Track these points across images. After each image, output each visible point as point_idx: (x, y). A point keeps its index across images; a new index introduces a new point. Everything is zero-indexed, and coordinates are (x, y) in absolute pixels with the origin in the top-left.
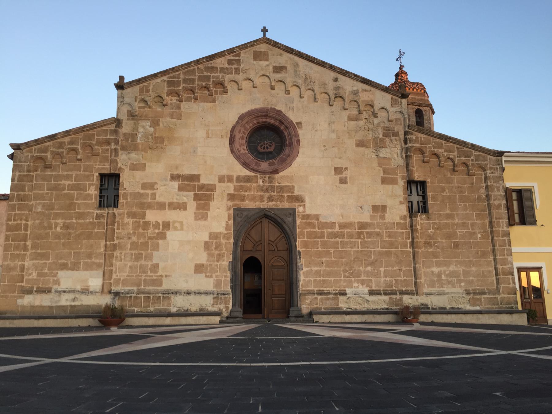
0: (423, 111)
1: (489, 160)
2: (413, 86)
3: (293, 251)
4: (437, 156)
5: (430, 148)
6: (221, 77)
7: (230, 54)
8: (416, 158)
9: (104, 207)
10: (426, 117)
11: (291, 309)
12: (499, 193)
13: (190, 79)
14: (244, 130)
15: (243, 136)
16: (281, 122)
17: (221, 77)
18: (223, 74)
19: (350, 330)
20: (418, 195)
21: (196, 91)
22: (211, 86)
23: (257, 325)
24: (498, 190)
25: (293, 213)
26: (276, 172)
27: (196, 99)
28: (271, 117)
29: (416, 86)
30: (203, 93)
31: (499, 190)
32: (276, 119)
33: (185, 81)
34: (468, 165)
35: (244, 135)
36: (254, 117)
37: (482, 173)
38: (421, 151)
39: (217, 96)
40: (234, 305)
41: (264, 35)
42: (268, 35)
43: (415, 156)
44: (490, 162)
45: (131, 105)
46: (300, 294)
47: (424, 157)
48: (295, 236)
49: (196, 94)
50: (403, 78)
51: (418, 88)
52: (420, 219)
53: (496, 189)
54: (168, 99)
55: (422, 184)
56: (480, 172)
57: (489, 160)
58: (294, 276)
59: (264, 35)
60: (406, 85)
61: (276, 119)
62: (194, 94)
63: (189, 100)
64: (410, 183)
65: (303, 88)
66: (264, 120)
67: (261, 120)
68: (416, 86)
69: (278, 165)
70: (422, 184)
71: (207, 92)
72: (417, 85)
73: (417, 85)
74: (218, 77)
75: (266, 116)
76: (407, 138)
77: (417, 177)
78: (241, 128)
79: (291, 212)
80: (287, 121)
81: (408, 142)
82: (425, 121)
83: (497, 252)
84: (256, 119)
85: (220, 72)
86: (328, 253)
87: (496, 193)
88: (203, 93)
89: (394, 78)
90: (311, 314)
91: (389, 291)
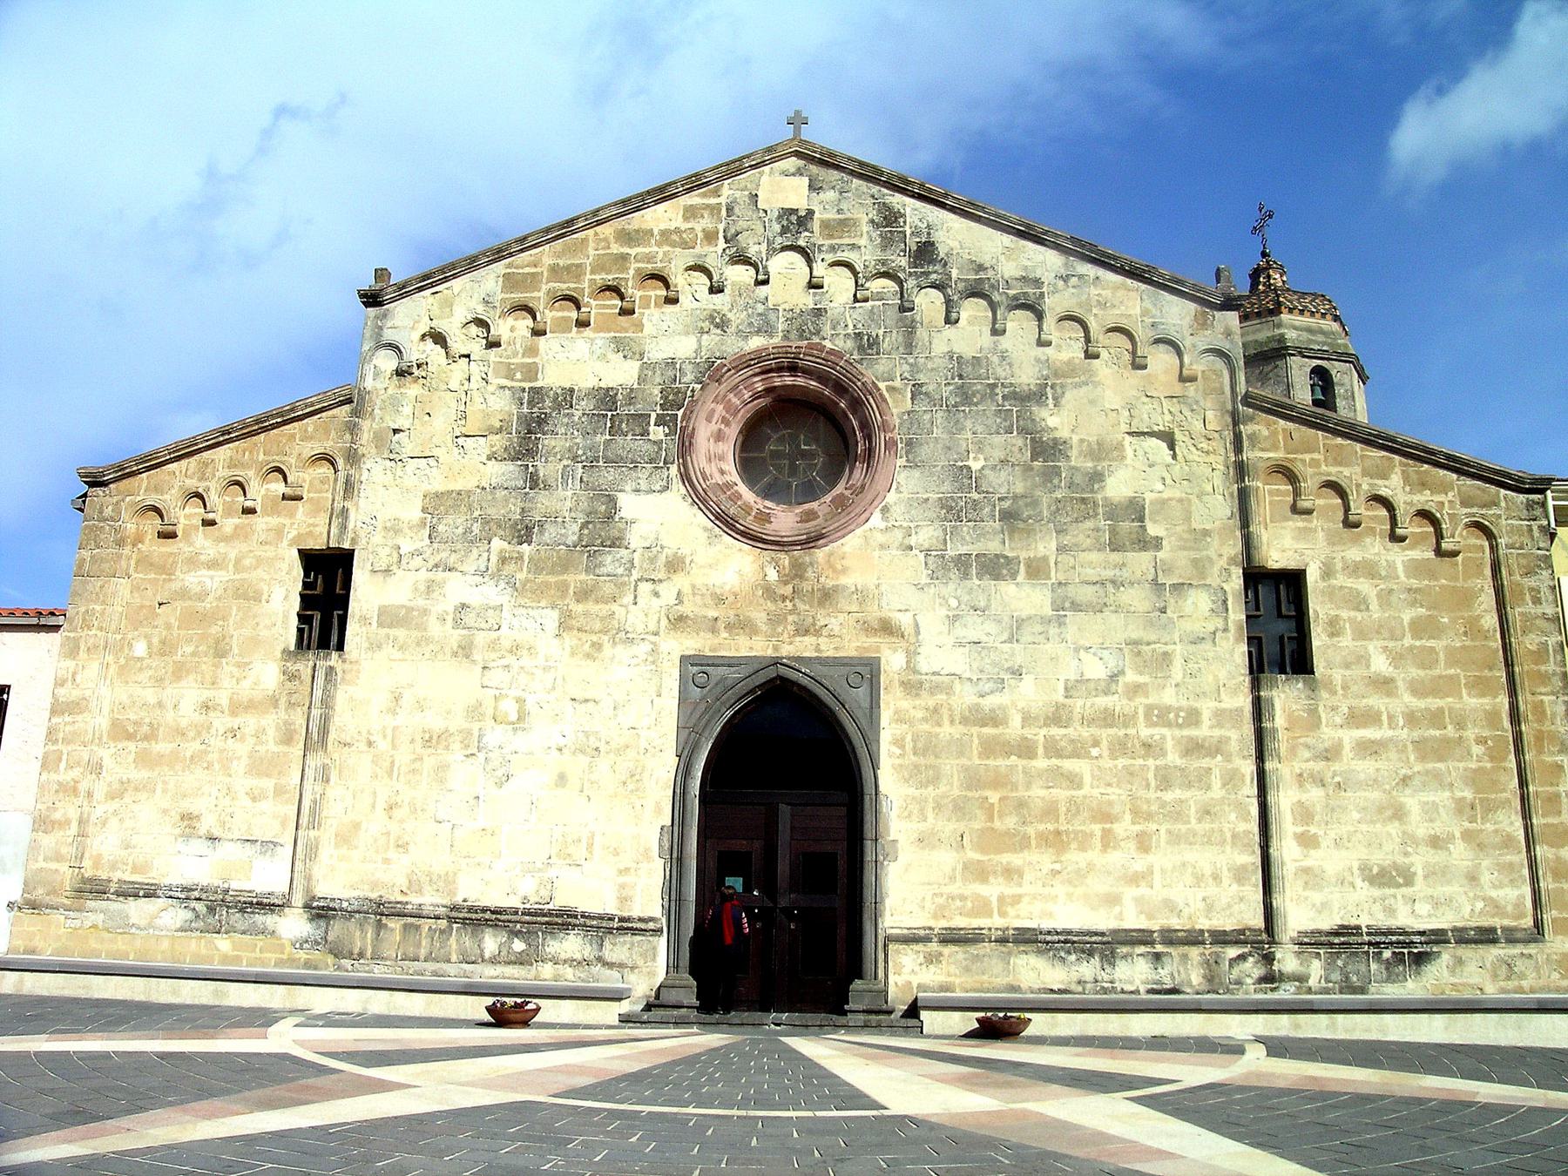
0: (1333, 373)
1: (1503, 504)
2: (1300, 303)
3: (867, 798)
4: (1335, 487)
5: (1315, 463)
6: (660, 256)
7: (690, 190)
8: (1269, 494)
9: (309, 648)
10: (1342, 391)
11: (857, 984)
12: (1539, 610)
13: (568, 268)
14: (724, 413)
15: (720, 430)
16: (840, 388)
17: (660, 256)
18: (669, 248)
19: (1193, 1007)
20: (1280, 615)
21: (586, 300)
22: (630, 284)
23: (781, 1038)
24: (1537, 601)
25: (868, 672)
26: (812, 541)
27: (583, 324)
28: (807, 372)
29: (1310, 303)
30: (605, 306)
31: (1539, 599)
32: (822, 378)
33: (555, 271)
34: (1438, 520)
35: (723, 426)
36: (757, 370)
37: (1482, 546)
38: (1288, 474)
39: (647, 312)
40: (673, 967)
41: (797, 131)
42: (807, 133)
43: (1270, 492)
44: (1508, 508)
45: (397, 348)
46: (889, 939)
47: (1297, 493)
48: (875, 748)
49: (583, 310)
50: (1272, 281)
51: (1315, 307)
52: (1285, 696)
53: (1528, 597)
54: (503, 328)
55: (1293, 580)
56: (1479, 542)
57: (1503, 504)
58: (869, 877)
59: (797, 131)
60: (1281, 299)
61: (822, 378)
62: (578, 308)
63: (562, 327)
64: (1256, 577)
65: (910, 283)
66: (789, 380)
67: (777, 382)
68: (1310, 303)
69: (826, 520)
70: (1293, 580)
71: (619, 303)
72: (1313, 300)
73: (1313, 300)
74: (650, 258)
75: (793, 369)
76: (1240, 432)
77: (1277, 553)
78: (713, 405)
79: (864, 671)
80: (859, 384)
81: (1246, 443)
82: (1338, 400)
83: (1537, 804)
84: (763, 377)
85: (659, 244)
86: (1201, 780)
87: (1530, 608)
88: (605, 306)
89: (1249, 281)
90: (913, 1011)
91: (1180, 934)
